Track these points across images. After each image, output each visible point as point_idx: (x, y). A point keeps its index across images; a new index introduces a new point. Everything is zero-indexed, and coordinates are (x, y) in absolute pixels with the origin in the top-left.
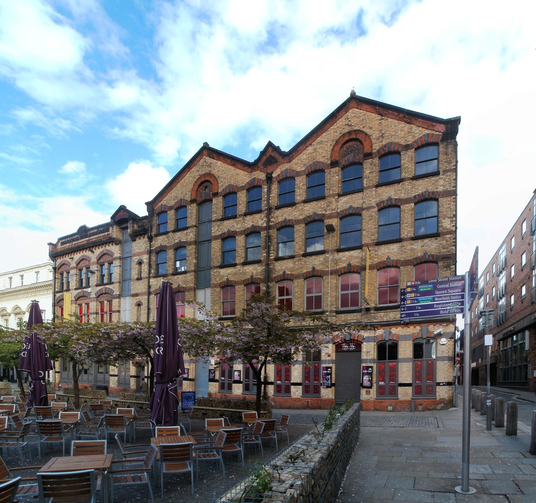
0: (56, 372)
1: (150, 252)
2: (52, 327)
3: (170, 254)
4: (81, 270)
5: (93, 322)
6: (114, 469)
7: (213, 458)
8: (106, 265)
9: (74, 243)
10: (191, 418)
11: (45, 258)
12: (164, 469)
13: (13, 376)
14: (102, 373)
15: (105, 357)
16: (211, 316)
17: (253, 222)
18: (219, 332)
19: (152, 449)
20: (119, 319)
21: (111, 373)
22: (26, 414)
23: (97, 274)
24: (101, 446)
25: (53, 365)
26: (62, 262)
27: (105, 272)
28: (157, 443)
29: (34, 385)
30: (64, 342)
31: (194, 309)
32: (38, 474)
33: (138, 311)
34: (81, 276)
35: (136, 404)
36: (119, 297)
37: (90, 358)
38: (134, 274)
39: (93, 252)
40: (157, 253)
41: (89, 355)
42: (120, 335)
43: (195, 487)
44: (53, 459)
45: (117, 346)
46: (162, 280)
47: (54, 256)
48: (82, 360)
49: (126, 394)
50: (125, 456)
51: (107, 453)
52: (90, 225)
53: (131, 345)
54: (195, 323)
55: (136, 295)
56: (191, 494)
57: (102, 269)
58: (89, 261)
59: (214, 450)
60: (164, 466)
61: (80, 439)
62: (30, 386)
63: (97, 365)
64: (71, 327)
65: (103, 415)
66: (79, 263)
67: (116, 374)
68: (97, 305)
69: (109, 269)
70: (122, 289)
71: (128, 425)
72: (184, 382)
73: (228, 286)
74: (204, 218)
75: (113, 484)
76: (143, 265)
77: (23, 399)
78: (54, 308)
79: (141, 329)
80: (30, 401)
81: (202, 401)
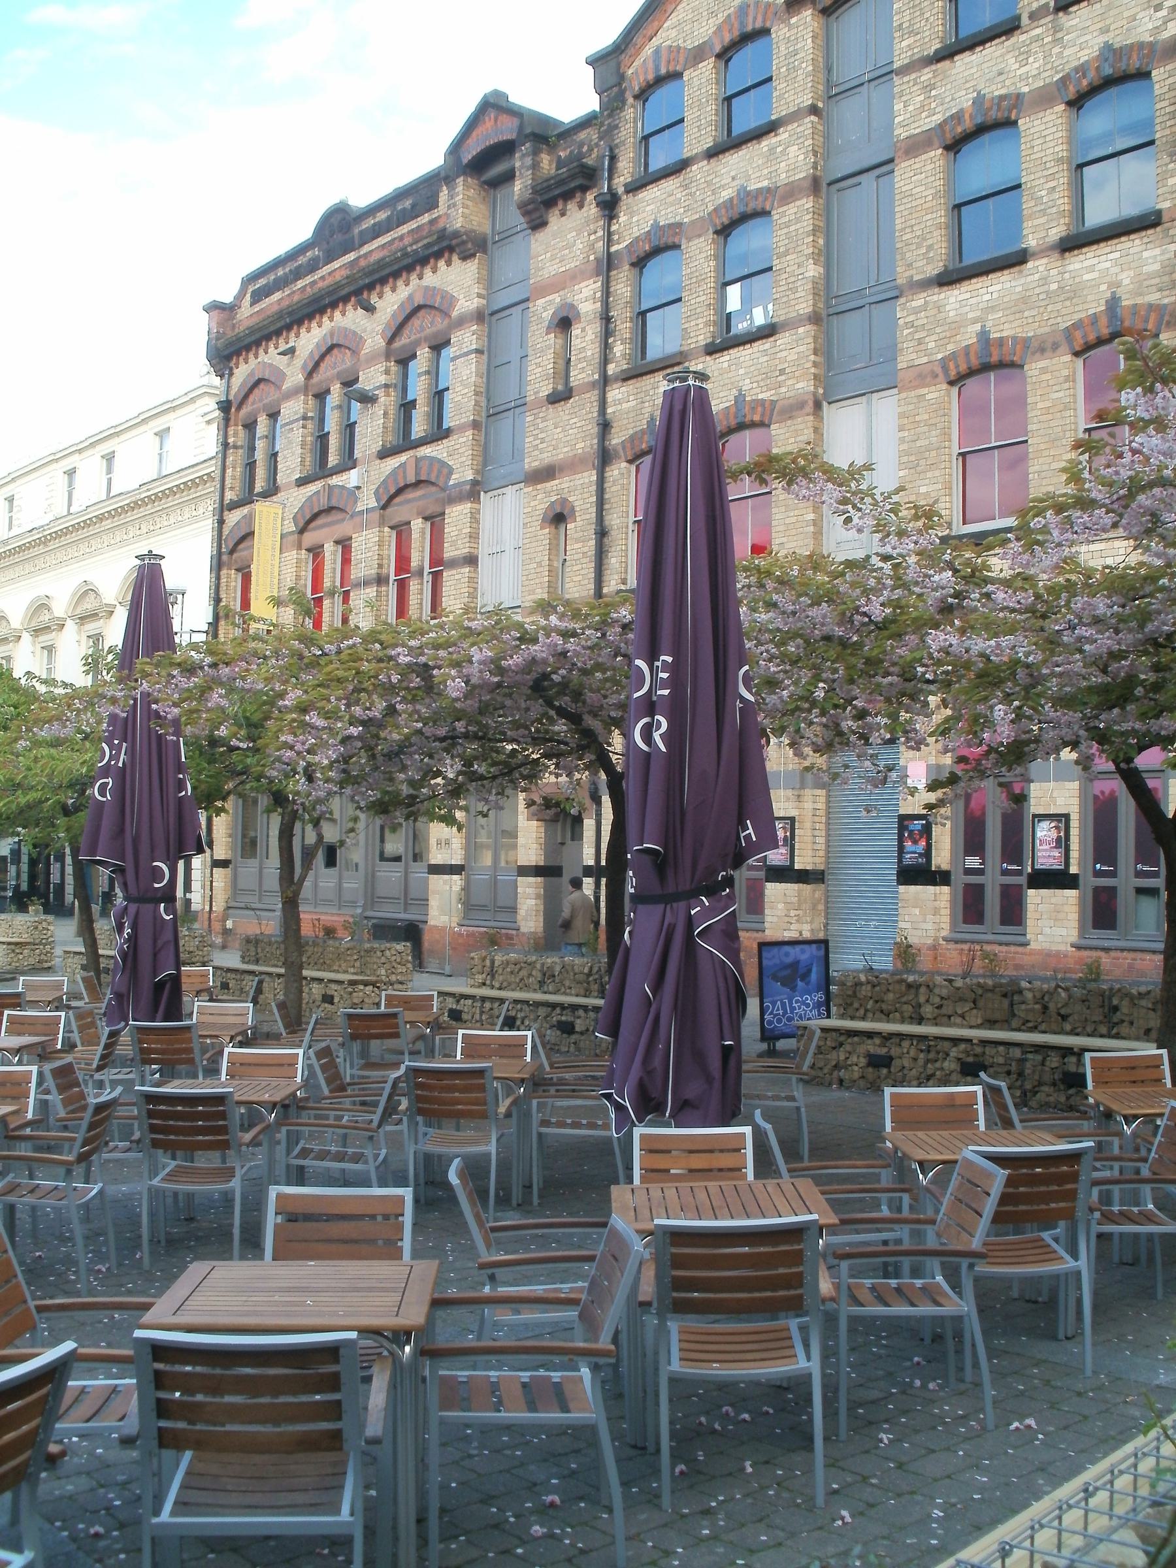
0: (217, 864)
1: (607, 265)
2: (208, 660)
3: (699, 254)
4: (321, 396)
5: (363, 621)
6: (442, 1340)
7: (926, 1309)
8: (423, 353)
9: (300, 284)
10: (812, 1081)
11: (193, 369)
12: (675, 1354)
13: (61, 887)
14: (398, 859)
15: (412, 783)
16: (901, 534)
17: (1105, 30)
18: (946, 610)
19: (618, 1250)
20: (473, 596)
21: (437, 857)
22: (103, 1057)
23: (387, 401)
24: (386, 1217)
25: (203, 834)
26: (251, 374)
27: (418, 389)
28: (640, 1212)
29: (134, 927)
30: (250, 725)
31: (817, 508)
32: (139, 1333)
33: (553, 548)
34: (322, 420)
35: (542, 1011)
36: (474, 491)
37: (348, 791)
38: (539, 378)
39: (370, 309)
40: (640, 264)
41: (347, 779)
42: (474, 670)
43: (832, 1463)
44: (197, 1269)
45: (460, 726)
46: (664, 386)
47: (224, 355)
48: (319, 801)
49: (499, 958)
50: (491, 1271)
51: (415, 1255)
52: (360, 200)
53: (530, 714)
54: (821, 578)
55: (546, 474)
56: (811, 1508)
57: (405, 376)
58: (355, 353)
59: (934, 1264)
60: (675, 1337)
61: (299, 1176)
62: (120, 928)
63: (379, 822)
64: (277, 654)
65: (396, 1065)
66: (317, 365)
67: (457, 860)
68: (380, 544)
69: (434, 372)
70: (485, 456)
71: (508, 1115)
72: (772, 890)
73: (987, 366)
74: (851, 68)
75: (438, 1414)
76: (576, 331)
77: (94, 987)
78: (218, 578)
79: (567, 634)
80: (119, 996)
81: (865, 991)
